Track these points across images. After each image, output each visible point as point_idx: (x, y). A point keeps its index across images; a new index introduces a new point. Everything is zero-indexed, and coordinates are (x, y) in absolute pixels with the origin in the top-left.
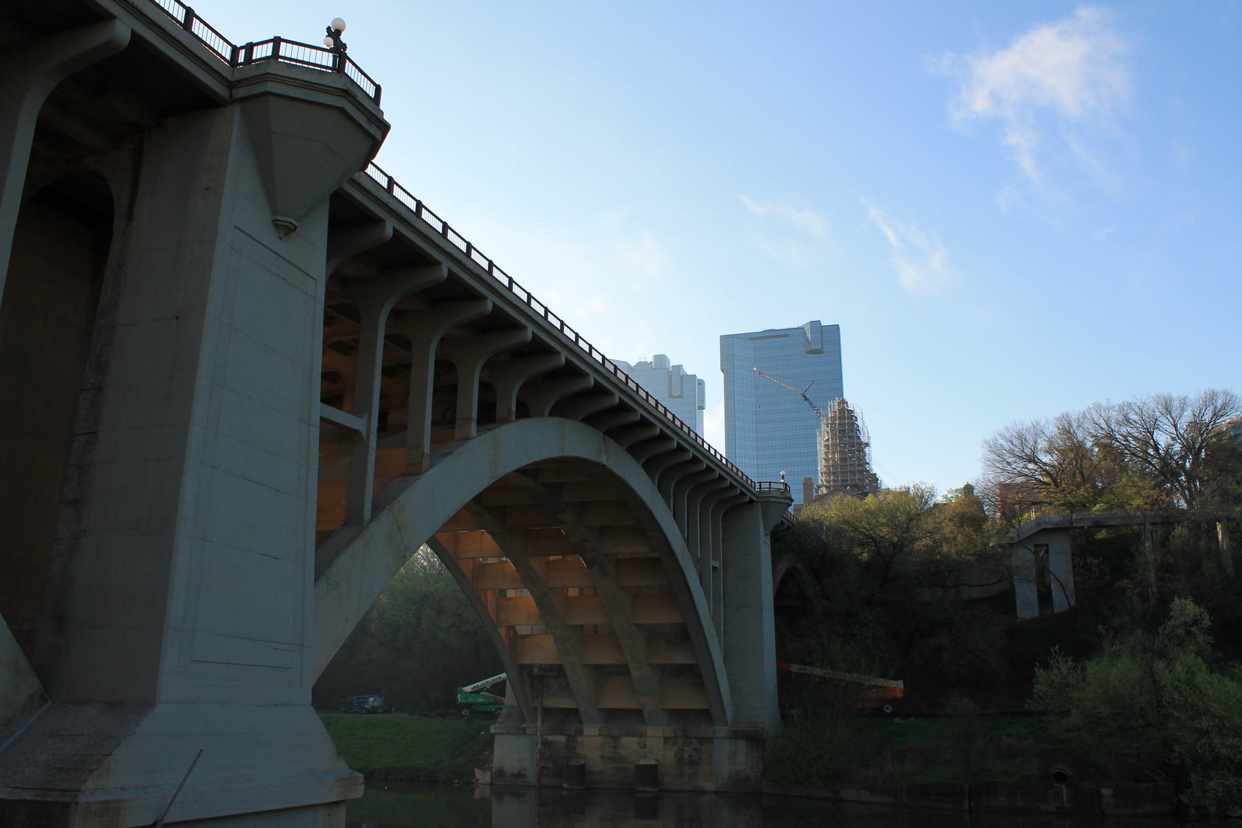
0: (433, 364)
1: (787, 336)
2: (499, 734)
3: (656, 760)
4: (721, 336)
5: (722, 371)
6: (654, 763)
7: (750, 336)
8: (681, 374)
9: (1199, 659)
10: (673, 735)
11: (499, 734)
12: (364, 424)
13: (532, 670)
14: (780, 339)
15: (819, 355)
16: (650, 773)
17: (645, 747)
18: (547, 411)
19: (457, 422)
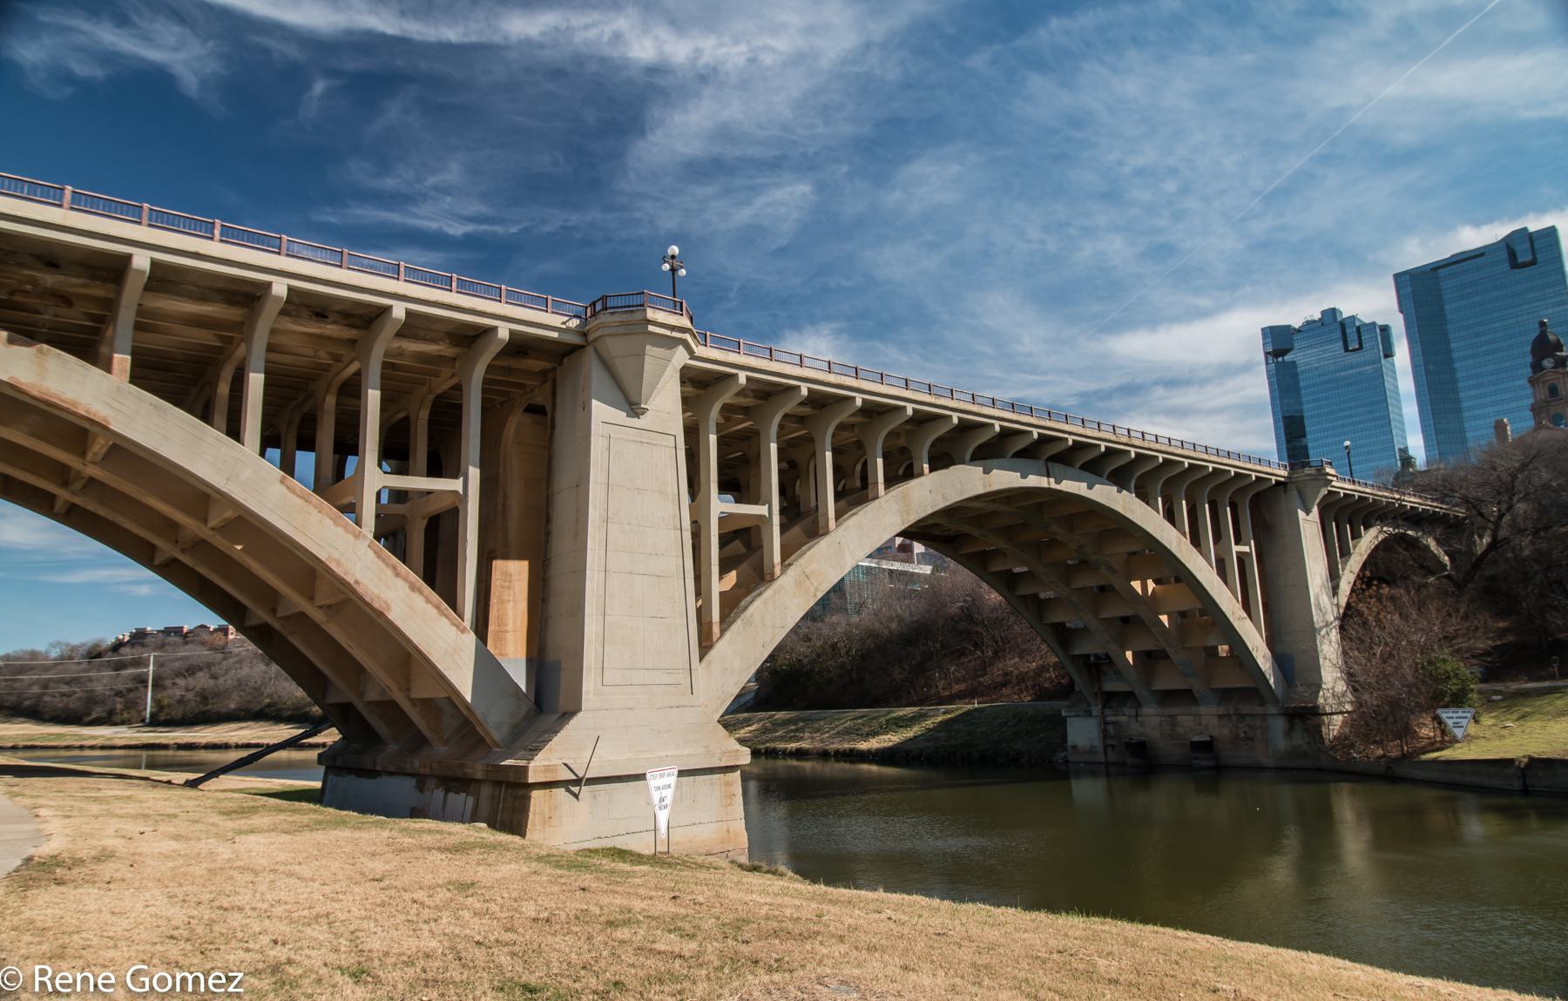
0: (716, 486)
1: (1482, 255)
2: (1070, 716)
3: (1211, 736)
4: (1394, 275)
5: (1401, 311)
6: (1209, 739)
7: (1431, 267)
8: (1358, 324)
9: (1081, 626)
10: (1226, 713)
11: (1070, 716)
12: (769, 509)
13: (1089, 660)
14: (1473, 261)
15: (1534, 267)
16: (1207, 747)
17: (1200, 724)
18: (968, 457)
19: (870, 487)
